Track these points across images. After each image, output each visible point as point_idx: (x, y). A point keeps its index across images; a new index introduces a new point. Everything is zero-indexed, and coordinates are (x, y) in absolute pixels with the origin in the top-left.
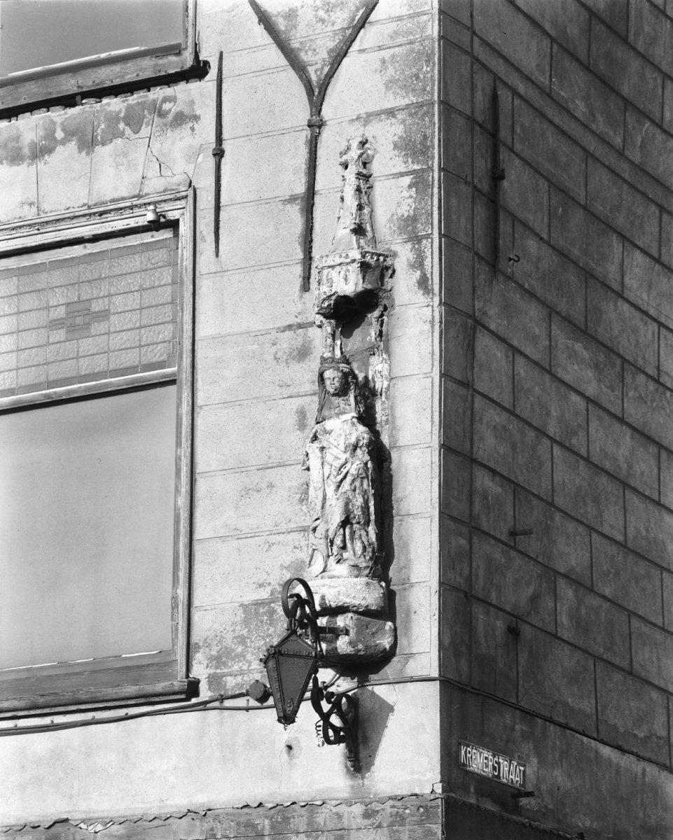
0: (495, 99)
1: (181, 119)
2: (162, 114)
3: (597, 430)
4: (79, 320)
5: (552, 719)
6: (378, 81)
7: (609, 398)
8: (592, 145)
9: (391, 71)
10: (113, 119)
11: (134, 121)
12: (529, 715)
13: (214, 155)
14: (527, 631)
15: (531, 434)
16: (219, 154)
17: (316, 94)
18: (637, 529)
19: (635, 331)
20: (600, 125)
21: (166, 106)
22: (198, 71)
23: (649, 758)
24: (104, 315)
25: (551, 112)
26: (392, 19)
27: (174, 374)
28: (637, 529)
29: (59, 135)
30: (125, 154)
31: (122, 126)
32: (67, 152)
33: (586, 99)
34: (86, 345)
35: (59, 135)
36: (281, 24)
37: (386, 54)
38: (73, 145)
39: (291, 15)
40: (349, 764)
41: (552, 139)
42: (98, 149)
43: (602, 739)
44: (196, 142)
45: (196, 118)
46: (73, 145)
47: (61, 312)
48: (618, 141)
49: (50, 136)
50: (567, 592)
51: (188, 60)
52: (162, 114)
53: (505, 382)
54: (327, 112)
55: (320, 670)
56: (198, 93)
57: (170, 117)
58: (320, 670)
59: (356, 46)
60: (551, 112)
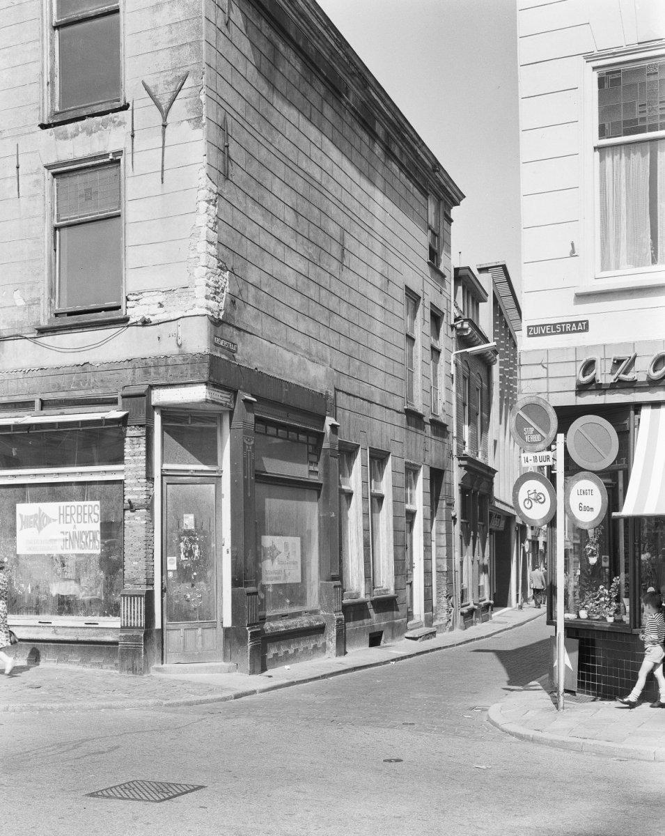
0: (225, 118)
1: (120, 124)
2: (114, 122)
3: (262, 236)
4: (89, 195)
6: (185, 110)
7: (266, 226)
8: (261, 140)
9: (189, 106)
10: (98, 124)
11: (104, 125)
12: (239, 329)
13: (29, 669)
14: (238, 301)
15: (239, 235)
16: (133, 136)
17: (165, 114)
18: (277, 271)
19: (276, 205)
20: (264, 133)
21: (115, 119)
22: (125, 107)
25: (246, 126)
27: (120, 213)
28: (277, 271)
29: (80, 130)
30: (102, 136)
31: (101, 126)
32: (83, 136)
33: (259, 123)
35: (80, 130)
36: (153, 90)
37: (188, 100)
38: (85, 133)
40: (93, 660)
41: (246, 135)
42: (93, 134)
45: (125, 123)
46: (85, 133)
48: (270, 140)
49: (77, 130)
50: (252, 289)
51: (122, 103)
52: (114, 122)
53: (230, 216)
54: (168, 120)
55: (17, 505)
57: (117, 123)
59: (178, 97)
60: (246, 126)
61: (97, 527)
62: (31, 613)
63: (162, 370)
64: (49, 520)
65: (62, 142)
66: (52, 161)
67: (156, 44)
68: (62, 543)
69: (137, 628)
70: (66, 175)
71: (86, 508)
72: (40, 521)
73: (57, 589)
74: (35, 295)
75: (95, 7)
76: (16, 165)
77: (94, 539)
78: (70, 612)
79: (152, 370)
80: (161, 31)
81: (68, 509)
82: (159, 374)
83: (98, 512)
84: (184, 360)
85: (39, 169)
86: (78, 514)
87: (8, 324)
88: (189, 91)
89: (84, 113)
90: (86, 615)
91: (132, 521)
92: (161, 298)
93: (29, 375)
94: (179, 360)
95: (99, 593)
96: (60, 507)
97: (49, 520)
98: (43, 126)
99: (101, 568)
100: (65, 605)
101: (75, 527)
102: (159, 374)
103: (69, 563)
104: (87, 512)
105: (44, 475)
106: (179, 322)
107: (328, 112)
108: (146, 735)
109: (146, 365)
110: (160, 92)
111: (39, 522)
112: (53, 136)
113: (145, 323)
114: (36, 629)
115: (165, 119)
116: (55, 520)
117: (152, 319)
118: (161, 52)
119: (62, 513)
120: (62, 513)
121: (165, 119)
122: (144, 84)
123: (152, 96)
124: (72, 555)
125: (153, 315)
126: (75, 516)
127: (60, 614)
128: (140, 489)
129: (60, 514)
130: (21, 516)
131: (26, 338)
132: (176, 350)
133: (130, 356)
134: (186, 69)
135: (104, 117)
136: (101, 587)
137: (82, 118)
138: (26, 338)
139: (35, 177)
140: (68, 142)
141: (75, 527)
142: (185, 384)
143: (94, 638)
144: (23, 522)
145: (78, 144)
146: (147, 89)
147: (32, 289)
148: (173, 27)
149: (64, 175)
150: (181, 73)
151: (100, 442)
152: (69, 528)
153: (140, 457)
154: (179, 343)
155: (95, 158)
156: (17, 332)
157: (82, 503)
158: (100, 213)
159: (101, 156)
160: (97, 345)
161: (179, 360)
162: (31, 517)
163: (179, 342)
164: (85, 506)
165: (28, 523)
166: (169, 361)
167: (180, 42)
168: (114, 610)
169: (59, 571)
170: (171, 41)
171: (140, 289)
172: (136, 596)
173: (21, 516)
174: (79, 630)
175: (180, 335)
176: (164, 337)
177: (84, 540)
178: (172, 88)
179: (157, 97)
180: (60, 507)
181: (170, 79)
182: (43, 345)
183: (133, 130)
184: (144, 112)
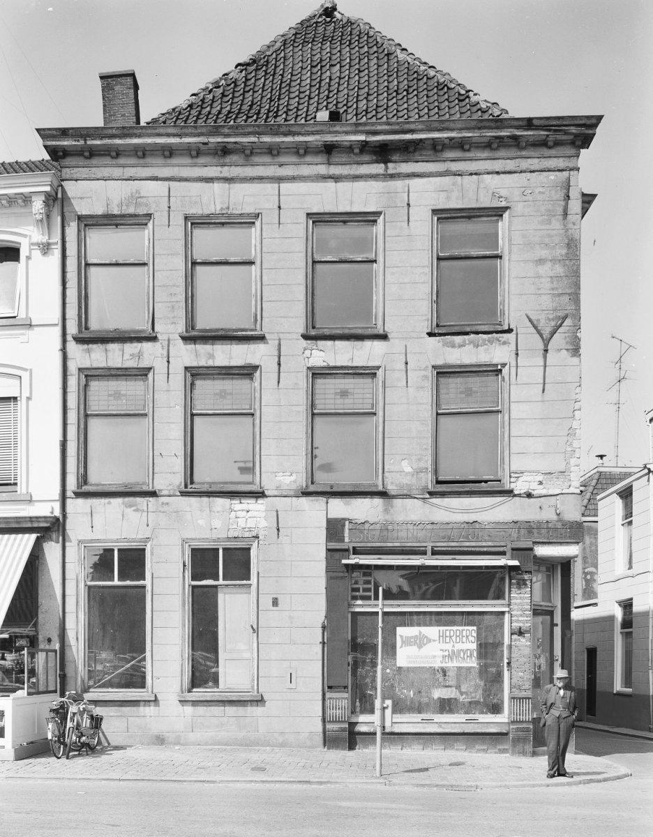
1: (504, 343)
5: (315, 458)
11: (491, 342)
17: (546, 343)
22: (510, 331)
23: (316, 457)
24: (336, 394)
26: (567, 326)
34: (347, 401)
36: (535, 323)
37: (567, 335)
39: (538, 320)
43: (316, 457)
44: (510, 349)
47: (218, 391)
49: (464, 341)
54: (549, 347)
55: (398, 628)
56: (511, 337)
58: (398, 628)
61: (474, 646)
62: (413, 713)
63: (543, 531)
64: (429, 641)
65: (450, 349)
66: (440, 362)
67: (539, 289)
68: (441, 659)
69: (526, 721)
70: (448, 375)
71: (464, 632)
72: (420, 641)
73: (438, 694)
74: (422, 465)
75: (477, 250)
76: (404, 360)
77: (471, 655)
78: (451, 711)
79: (535, 531)
80: (543, 280)
81: (448, 632)
82: (541, 534)
83: (475, 635)
84: (563, 525)
85: (427, 367)
86: (457, 636)
87: (396, 485)
88: (568, 328)
89: (468, 329)
90: (466, 713)
91: (518, 643)
92: (540, 478)
93: (420, 527)
94: (559, 525)
95: (479, 696)
96: (439, 631)
97: (429, 641)
98: (430, 334)
99: (481, 678)
100: (446, 706)
101: (453, 646)
102: (541, 534)
103: (451, 674)
104: (464, 634)
105: (428, 606)
106: (558, 497)
107: (47, 584)
108: (175, 686)
109: (530, 528)
110: (541, 324)
111: (420, 642)
112: (441, 344)
113: (529, 495)
114: (420, 725)
115: (546, 345)
116: (434, 641)
117: (533, 492)
118: (543, 296)
119: (441, 635)
120: (441, 635)
121: (546, 345)
122: (528, 317)
123: (535, 327)
124: (453, 667)
125: (533, 490)
126: (454, 638)
127: (442, 713)
128: (526, 618)
129: (440, 636)
130: (401, 636)
131: (415, 498)
132: (555, 517)
133: (516, 519)
134: (566, 312)
135: (490, 336)
136: (480, 692)
137: (467, 333)
138: (415, 498)
139: (423, 373)
140: (456, 350)
141: (453, 646)
142: (561, 543)
143: (479, 731)
144: (403, 642)
145: (463, 353)
146: (530, 321)
147: (419, 460)
148: (555, 279)
149: (445, 375)
150: (561, 314)
151: (481, 584)
152: (449, 647)
153: (526, 595)
154: (558, 512)
155: (480, 366)
156: (405, 492)
157: (460, 628)
158: (480, 408)
159: (485, 365)
160: (484, 509)
161: (559, 525)
162: (412, 637)
163: (558, 512)
164: (463, 630)
165: (408, 642)
166: (550, 525)
167: (560, 291)
168: (496, 709)
169: (441, 679)
170: (553, 289)
171: (522, 469)
172: (525, 698)
173: (401, 636)
174: (462, 725)
175: (558, 506)
176: (544, 507)
177: (462, 656)
178: (553, 323)
179: (539, 328)
180: (439, 631)
181: (551, 317)
182: (433, 505)
183: (517, 350)
184: (529, 340)
